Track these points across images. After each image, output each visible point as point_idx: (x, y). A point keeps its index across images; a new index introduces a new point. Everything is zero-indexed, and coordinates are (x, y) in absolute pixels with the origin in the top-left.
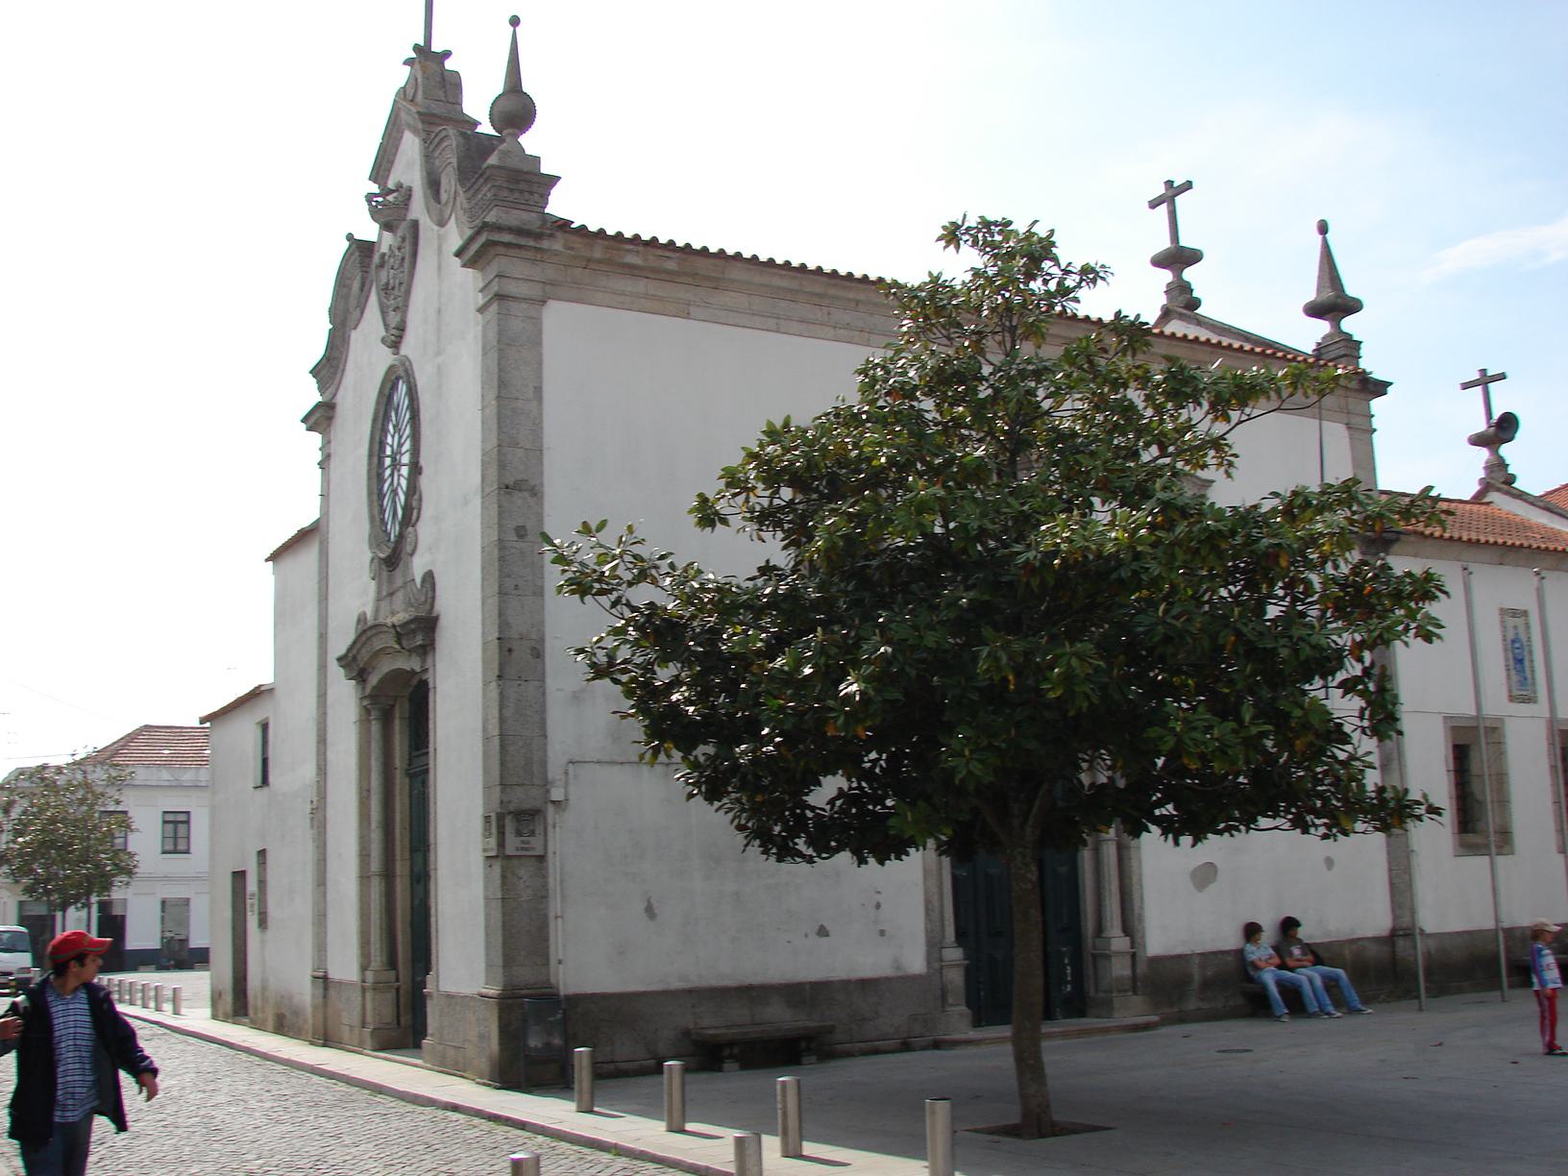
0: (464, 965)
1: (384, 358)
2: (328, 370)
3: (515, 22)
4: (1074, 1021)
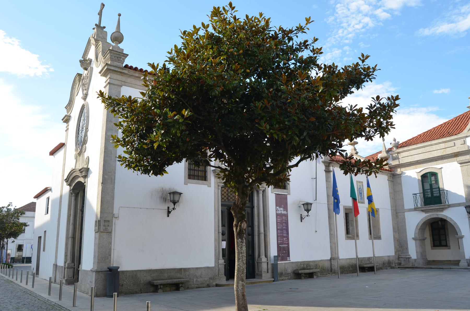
0: (88, 262)
1: (82, 102)
2: (69, 106)
3: (120, 15)
4: (252, 279)
